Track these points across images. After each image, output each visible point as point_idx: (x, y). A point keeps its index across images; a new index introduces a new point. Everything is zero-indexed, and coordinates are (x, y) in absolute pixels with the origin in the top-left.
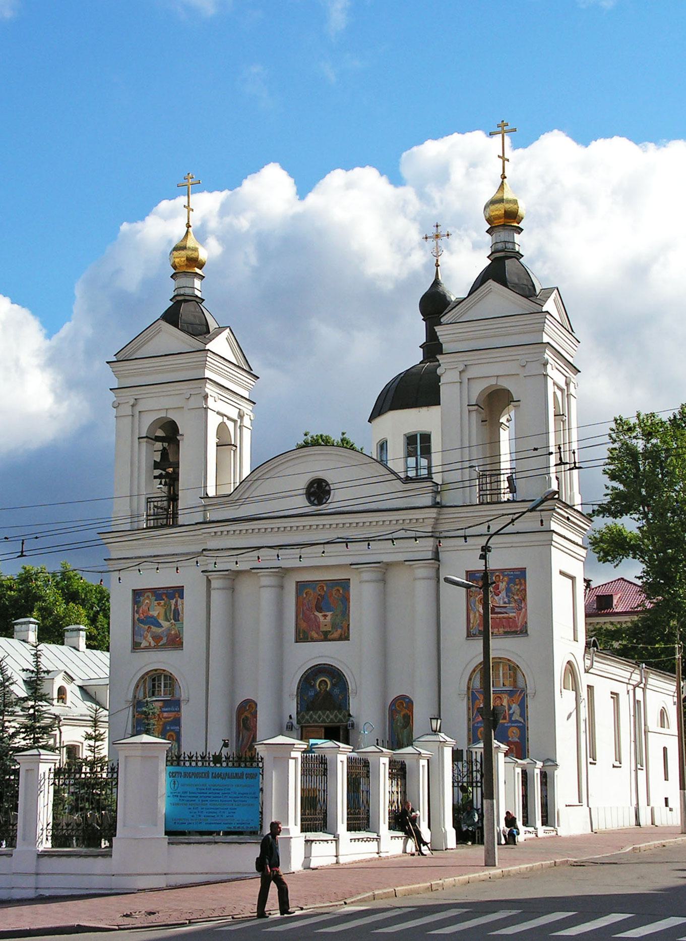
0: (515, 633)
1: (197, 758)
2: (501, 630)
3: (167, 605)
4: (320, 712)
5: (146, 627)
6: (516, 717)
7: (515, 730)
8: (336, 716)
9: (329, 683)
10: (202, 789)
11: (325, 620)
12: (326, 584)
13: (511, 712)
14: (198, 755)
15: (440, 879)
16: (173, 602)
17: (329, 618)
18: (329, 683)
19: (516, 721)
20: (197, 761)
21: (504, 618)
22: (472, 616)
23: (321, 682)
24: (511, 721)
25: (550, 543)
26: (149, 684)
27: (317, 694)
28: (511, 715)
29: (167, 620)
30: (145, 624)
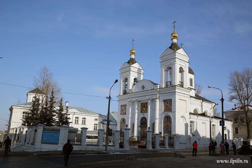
11: (144, 109)
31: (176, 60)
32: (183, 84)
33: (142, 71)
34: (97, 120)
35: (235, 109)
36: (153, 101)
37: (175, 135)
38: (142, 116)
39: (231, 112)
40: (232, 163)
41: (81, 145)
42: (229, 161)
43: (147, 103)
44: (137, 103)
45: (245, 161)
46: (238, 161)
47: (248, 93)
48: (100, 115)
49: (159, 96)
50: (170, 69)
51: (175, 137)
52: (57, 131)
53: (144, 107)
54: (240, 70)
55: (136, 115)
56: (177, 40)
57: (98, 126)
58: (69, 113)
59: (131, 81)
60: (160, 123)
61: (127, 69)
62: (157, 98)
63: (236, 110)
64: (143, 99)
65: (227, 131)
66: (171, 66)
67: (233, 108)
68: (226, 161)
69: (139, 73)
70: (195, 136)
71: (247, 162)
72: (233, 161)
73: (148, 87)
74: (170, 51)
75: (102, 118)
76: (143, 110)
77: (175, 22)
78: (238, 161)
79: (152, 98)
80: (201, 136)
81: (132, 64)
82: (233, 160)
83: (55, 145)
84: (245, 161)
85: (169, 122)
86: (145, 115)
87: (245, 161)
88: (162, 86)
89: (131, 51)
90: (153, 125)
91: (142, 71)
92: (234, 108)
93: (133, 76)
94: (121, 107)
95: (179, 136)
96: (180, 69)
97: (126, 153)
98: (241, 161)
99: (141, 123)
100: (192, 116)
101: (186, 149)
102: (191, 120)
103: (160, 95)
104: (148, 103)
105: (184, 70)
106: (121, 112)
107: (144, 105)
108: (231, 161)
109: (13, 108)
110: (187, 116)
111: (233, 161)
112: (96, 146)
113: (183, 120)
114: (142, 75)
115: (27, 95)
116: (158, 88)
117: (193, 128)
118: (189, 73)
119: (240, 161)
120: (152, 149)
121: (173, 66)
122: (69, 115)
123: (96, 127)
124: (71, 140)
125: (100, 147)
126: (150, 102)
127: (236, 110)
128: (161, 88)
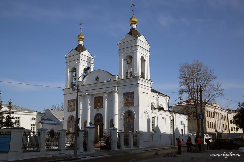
0: (132, 105)
3: (73, 103)
6: (132, 123)
11: (99, 104)
15: (193, 158)
19: (132, 124)
20: (26, 133)
25: (138, 86)
28: (131, 122)
31: (138, 48)
32: (144, 75)
33: (93, 60)
34: (34, 119)
35: (181, 103)
36: (111, 94)
37: (139, 132)
38: (96, 112)
39: (177, 106)
40: (225, 157)
41: (39, 151)
42: (222, 155)
43: (102, 97)
44: (90, 97)
45: (238, 155)
46: (231, 155)
47: (197, 86)
48: (39, 113)
49: (118, 88)
50: (130, 59)
51: (139, 134)
52: (5, 135)
53: (98, 102)
54: (190, 62)
55: (89, 112)
56: (137, 25)
57: (35, 127)
58: (12, 111)
59: (81, 71)
60: (120, 119)
61: (76, 57)
62: (115, 92)
63: (182, 104)
64: (98, 93)
65: (183, 126)
66: (131, 54)
67: (178, 102)
68: (219, 155)
69: (89, 62)
70: (156, 132)
71: (240, 156)
72: (226, 155)
73: (104, 78)
74: (130, 37)
75: (41, 117)
76: (97, 105)
78: (231, 155)
79: (109, 91)
80: (162, 132)
81: (82, 52)
82: (226, 154)
83: (4, 154)
84: (237, 154)
85: (131, 118)
86: (100, 111)
87: (238, 155)
88: (122, 77)
89: (79, 36)
90: (111, 123)
91: (93, 60)
92: (180, 102)
93: (83, 65)
94: (69, 103)
95: (143, 134)
97: (99, 157)
98: (233, 154)
99: (94, 121)
100: (155, 111)
101: (150, 147)
102: (153, 115)
103: (118, 87)
104: (104, 98)
106: (68, 108)
107: (99, 100)
108: (224, 155)
110: (149, 110)
111: (226, 155)
112: (57, 151)
113: (146, 116)
114: (92, 65)
116: (117, 79)
117: (154, 124)
119: (232, 155)
120: (118, 150)
121: (135, 54)
122: (13, 113)
123: (34, 128)
125: (62, 152)
126: (106, 95)
127: (182, 104)
128: (120, 80)
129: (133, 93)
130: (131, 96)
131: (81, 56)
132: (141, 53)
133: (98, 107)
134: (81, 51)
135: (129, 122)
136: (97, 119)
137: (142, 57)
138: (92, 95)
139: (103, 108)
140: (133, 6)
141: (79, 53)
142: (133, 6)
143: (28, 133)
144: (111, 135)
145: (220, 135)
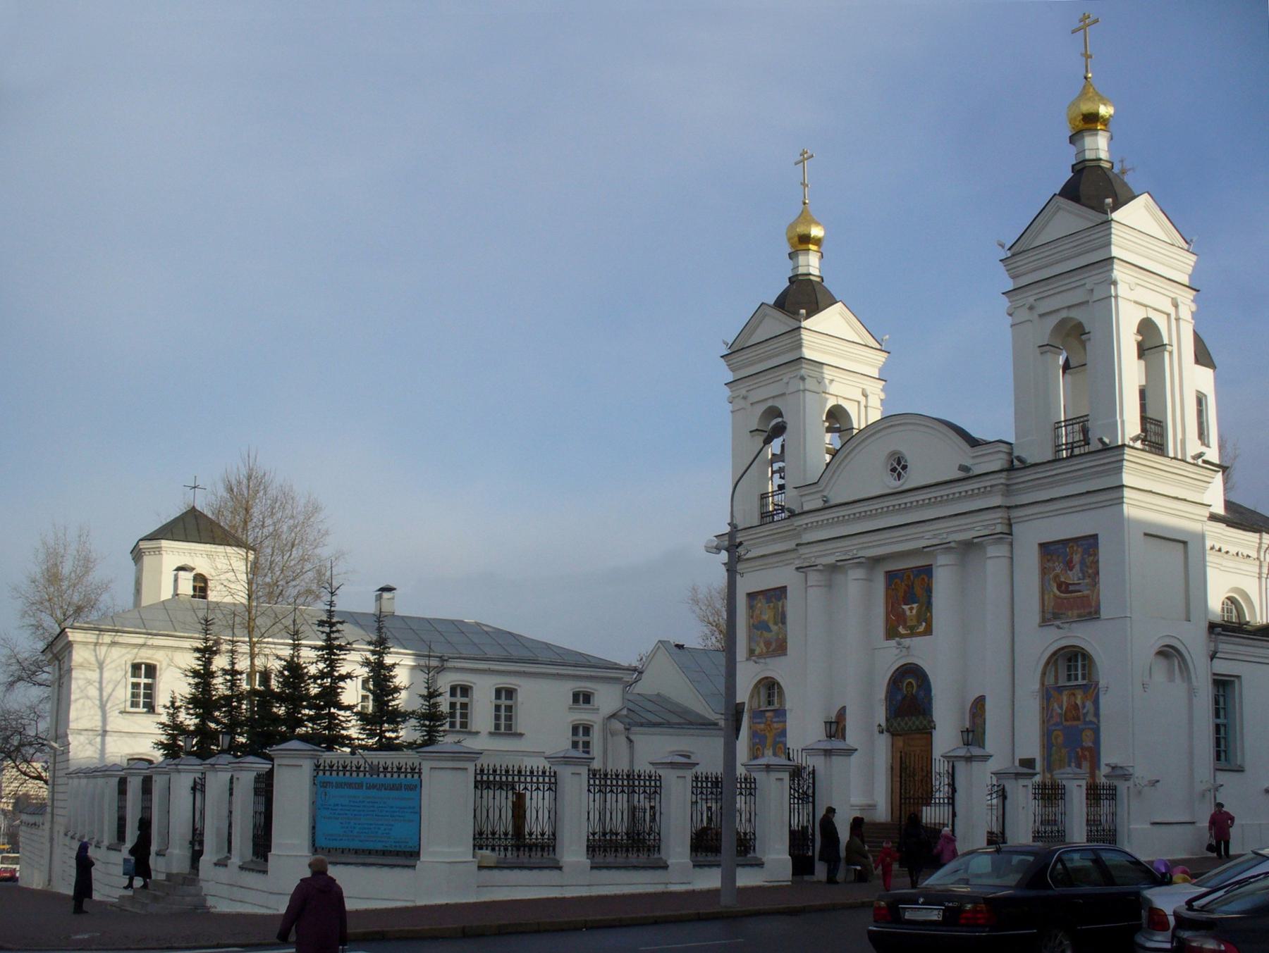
1: (406, 769)
2: (1076, 612)
4: (906, 718)
5: (759, 633)
6: (1090, 718)
7: (1089, 733)
8: (921, 723)
9: (915, 685)
10: (354, 802)
11: (911, 610)
12: (913, 572)
13: (1085, 711)
14: (394, 766)
16: (780, 604)
17: (914, 611)
18: (915, 685)
19: (1091, 722)
21: (1078, 597)
22: (1046, 597)
23: (907, 684)
24: (1085, 723)
26: (763, 692)
27: (904, 698)
28: (1085, 715)
29: (776, 624)
30: (758, 629)
32: (1162, 434)
51: (1127, 784)
56: (1111, 138)
74: (1072, 218)
76: (901, 619)
77: (1086, 23)
81: (809, 316)
83: (373, 869)
96: (1139, 331)
102: (1222, 667)
105: (1166, 341)
107: (910, 587)
109: (69, 645)
115: (137, 555)
118: (1198, 361)
124: (493, 833)
129: (1090, 543)
130: (1082, 562)
131: (805, 335)
132: (1136, 302)
133: (905, 627)
134: (803, 311)
135: (1074, 713)
136: (899, 698)
137: (1147, 327)
138: (877, 561)
139: (931, 633)
140: (803, 161)
141: (794, 324)
142: (803, 161)
143: (655, 780)
144: (954, 791)
145: (134, 785)
